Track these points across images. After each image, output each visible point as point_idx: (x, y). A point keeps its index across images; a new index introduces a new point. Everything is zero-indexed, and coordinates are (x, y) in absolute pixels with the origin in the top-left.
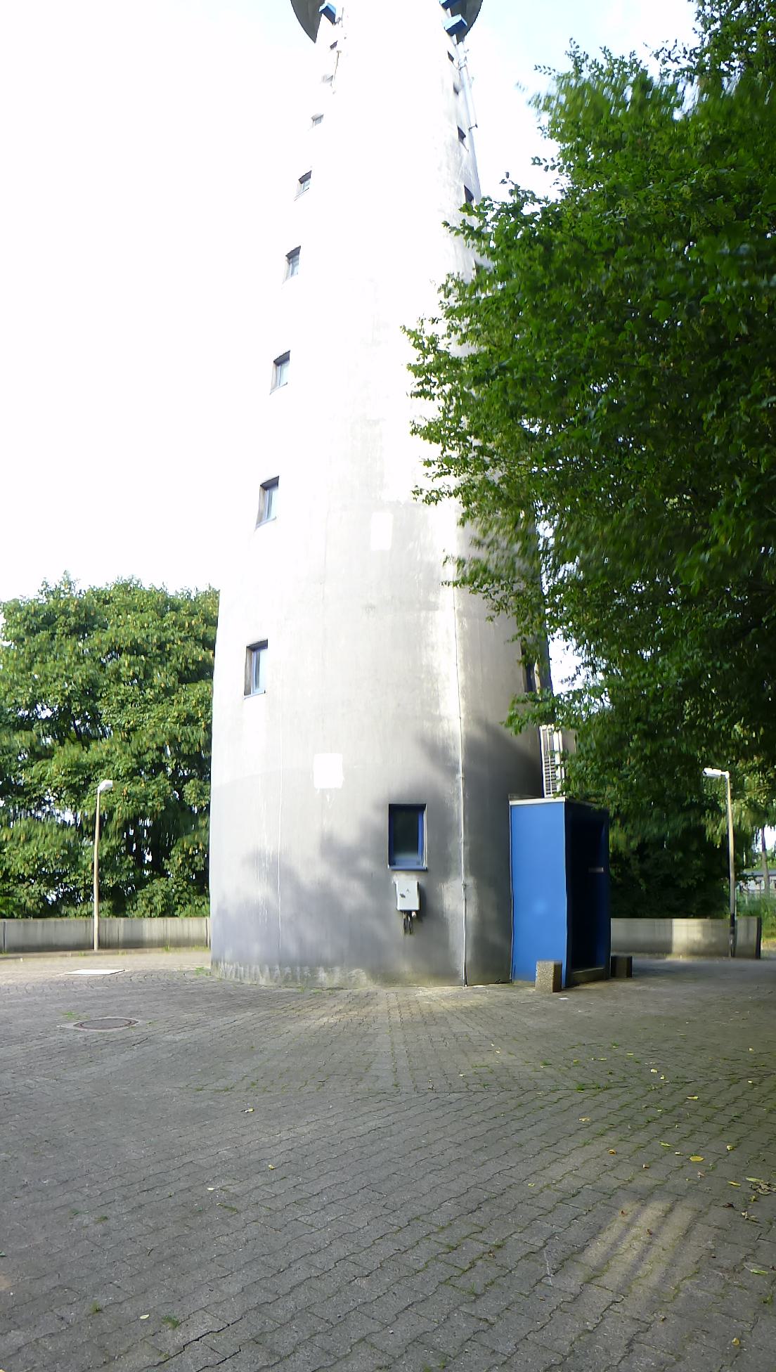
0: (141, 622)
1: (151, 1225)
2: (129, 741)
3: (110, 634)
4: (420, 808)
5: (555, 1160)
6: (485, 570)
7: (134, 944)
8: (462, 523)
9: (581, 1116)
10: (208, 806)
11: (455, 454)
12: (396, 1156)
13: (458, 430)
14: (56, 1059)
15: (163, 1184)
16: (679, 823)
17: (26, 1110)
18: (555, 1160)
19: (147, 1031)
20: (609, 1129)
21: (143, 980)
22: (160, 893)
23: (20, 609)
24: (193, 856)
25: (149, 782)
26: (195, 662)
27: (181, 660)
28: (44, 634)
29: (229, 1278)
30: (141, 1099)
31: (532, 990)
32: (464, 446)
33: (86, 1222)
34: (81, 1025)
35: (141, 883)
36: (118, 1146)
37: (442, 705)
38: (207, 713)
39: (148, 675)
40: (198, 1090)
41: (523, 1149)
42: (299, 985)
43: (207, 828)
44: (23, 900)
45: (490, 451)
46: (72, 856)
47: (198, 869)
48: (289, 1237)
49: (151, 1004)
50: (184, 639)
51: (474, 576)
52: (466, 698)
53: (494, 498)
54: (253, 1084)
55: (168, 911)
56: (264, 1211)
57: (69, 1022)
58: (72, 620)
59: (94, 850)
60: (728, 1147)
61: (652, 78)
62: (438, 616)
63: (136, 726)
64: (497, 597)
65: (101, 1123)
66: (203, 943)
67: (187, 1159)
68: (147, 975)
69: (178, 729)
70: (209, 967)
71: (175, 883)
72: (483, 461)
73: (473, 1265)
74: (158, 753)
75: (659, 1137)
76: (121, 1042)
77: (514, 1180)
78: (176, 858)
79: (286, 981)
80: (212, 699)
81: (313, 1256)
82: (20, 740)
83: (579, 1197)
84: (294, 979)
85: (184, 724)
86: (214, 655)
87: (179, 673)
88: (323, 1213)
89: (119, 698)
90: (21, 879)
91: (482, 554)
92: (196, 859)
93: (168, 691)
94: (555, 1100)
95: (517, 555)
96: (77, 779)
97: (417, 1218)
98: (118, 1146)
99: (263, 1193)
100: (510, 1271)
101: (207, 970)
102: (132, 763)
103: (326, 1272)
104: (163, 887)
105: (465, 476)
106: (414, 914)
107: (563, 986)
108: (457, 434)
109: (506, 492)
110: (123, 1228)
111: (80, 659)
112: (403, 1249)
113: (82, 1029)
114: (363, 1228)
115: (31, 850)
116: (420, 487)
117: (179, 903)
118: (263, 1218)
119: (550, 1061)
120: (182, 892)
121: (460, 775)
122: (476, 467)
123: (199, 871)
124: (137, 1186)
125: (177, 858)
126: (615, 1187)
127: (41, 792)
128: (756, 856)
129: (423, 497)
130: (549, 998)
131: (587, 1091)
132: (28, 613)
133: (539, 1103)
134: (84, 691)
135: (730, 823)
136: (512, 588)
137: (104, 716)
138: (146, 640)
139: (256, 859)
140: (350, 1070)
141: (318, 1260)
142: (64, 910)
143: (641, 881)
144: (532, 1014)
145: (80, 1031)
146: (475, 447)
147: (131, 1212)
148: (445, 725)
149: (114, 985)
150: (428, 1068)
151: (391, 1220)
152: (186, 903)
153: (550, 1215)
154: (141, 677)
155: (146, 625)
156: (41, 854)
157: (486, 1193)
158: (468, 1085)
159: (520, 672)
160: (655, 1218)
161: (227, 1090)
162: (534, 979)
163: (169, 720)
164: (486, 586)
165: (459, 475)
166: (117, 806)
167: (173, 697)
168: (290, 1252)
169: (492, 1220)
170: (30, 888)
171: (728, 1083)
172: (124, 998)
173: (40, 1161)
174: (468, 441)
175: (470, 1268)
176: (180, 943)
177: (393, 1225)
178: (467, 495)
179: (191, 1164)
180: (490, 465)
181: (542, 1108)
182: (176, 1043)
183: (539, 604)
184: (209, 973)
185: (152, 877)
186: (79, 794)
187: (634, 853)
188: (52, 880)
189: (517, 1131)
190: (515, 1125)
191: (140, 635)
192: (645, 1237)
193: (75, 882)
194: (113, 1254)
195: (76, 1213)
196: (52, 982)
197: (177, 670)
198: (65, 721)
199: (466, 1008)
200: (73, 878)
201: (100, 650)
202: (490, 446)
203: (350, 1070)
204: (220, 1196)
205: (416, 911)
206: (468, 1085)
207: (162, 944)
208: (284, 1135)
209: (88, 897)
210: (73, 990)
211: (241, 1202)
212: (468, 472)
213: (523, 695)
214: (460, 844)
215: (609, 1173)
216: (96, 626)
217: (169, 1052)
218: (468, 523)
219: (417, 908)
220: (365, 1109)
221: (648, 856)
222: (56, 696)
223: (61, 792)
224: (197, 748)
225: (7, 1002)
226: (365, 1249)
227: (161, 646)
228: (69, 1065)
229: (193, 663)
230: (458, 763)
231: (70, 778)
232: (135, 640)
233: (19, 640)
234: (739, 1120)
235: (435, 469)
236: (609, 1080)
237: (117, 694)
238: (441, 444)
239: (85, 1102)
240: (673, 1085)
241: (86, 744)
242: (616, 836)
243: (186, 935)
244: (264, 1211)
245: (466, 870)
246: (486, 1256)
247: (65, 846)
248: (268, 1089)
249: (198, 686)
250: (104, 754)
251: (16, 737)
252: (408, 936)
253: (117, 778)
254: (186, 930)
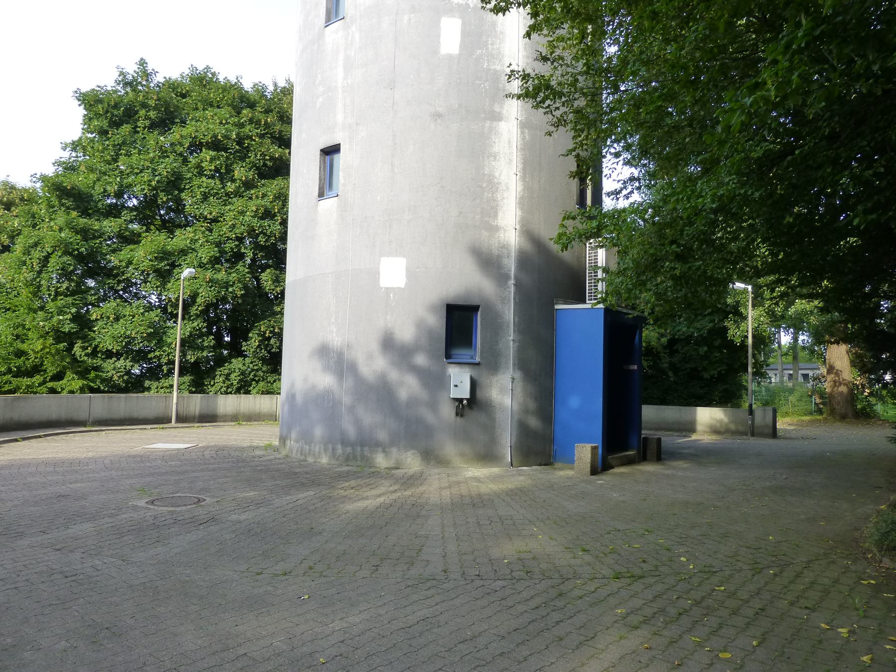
2: (211, 231)
3: (189, 130)
4: (475, 309)
7: (208, 418)
8: (528, 35)
9: (616, 607)
10: (283, 293)
12: (443, 649)
16: (705, 325)
20: (644, 622)
22: (237, 371)
24: (269, 339)
25: (229, 271)
26: (272, 158)
28: (126, 129)
30: (202, 583)
34: (152, 502)
35: (220, 361)
36: (176, 635)
37: (500, 215)
38: (283, 208)
39: (229, 170)
40: (258, 574)
42: (359, 463)
46: (157, 335)
47: (273, 350)
49: (220, 480)
50: (262, 136)
51: (537, 89)
52: (522, 209)
53: (562, 11)
54: (311, 568)
55: (244, 388)
57: (141, 499)
59: (178, 331)
60: (755, 643)
61: (306, 379)
63: (218, 217)
64: (558, 113)
66: (272, 417)
67: (241, 651)
68: (219, 449)
69: (256, 223)
70: (276, 442)
74: (237, 243)
75: (690, 630)
76: (188, 521)
78: (253, 340)
79: (347, 459)
82: (110, 225)
84: (355, 458)
85: (262, 218)
86: (290, 153)
87: (258, 168)
89: (202, 190)
90: (109, 354)
91: (545, 69)
92: (272, 341)
95: (580, 73)
96: (163, 264)
98: (176, 635)
101: (275, 446)
102: (215, 251)
104: (240, 366)
106: (465, 402)
107: (599, 469)
113: (152, 507)
115: (119, 328)
117: (253, 380)
119: (588, 547)
121: (512, 282)
123: (274, 352)
125: (253, 342)
127: (129, 275)
128: (773, 351)
131: (623, 580)
133: (577, 593)
135: (750, 325)
136: (572, 106)
137: (188, 206)
138: (227, 137)
139: (323, 351)
142: (147, 383)
143: (671, 374)
145: (150, 509)
150: (476, 553)
152: (259, 380)
158: (512, 571)
163: (248, 213)
164: (548, 102)
166: (200, 291)
167: (252, 192)
171: (753, 572)
172: (196, 474)
173: (98, 651)
176: (251, 418)
182: (241, 522)
184: (276, 450)
185: (231, 356)
187: (665, 348)
189: (557, 623)
190: (556, 616)
191: (220, 131)
196: (129, 456)
197: (255, 166)
198: (150, 210)
199: (511, 490)
200: (157, 353)
201: (181, 144)
205: (467, 399)
206: (512, 571)
207: (235, 418)
208: (337, 625)
209: (170, 372)
210: (149, 464)
213: (574, 208)
214: (510, 341)
216: (178, 120)
217: (233, 532)
219: (468, 397)
220: (415, 597)
221: (677, 351)
222: (143, 187)
223: (148, 274)
224: (272, 240)
227: (240, 142)
229: (270, 160)
230: (511, 271)
231: (156, 263)
232: (215, 136)
233: (103, 133)
234: (763, 613)
236: (642, 569)
239: (148, 585)
240: (701, 575)
242: (650, 334)
243: (258, 410)
245: (514, 365)
247: (151, 325)
248: (324, 574)
249: (276, 182)
250: (188, 241)
252: (458, 419)
253: (201, 265)
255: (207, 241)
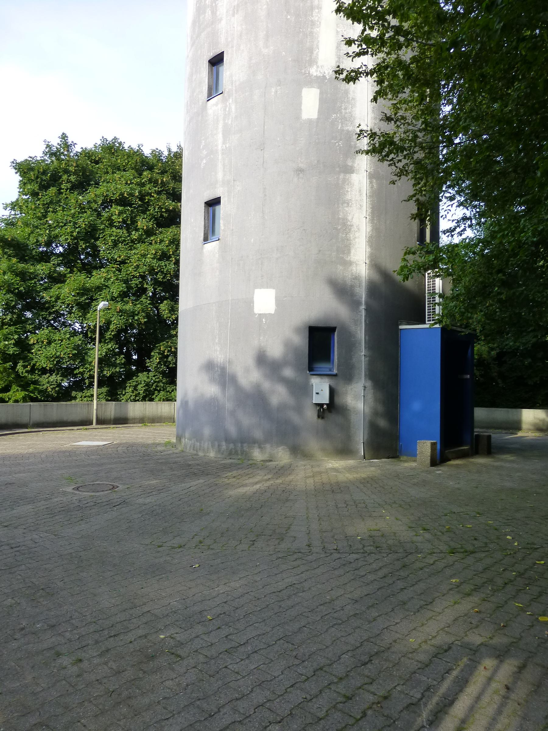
0: (125, 179)
1: (114, 668)
2: (120, 271)
3: (102, 189)
5: (431, 618)
6: (392, 143)
8: (375, 99)
9: (451, 577)
10: (177, 319)
11: (374, 34)
12: (307, 610)
13: (380, 9)
14: (57, 517)
15: (126, 631)
17: (30, 561)
18: (431, 618)
19: (125, 494)
20: (475, 590)
21: (126, 451)
22: (143, 383)
23: (32, 169)
24: (167, 356)
26: (167, 211)
27: (156, 210)
28: (52, 190)
29: (171, 720)
30: (115, 554)
31: (414, 464)
32: (383, 26)
33: (65, 663)
34: (77, 489)
35: (130, 375)
36: (95, 595)
38: (176, 251)
39: (134, 222)
40: (159, 547)
41: (406, 607)
42: (240, 457)
43: (176, 336)
44: (45, 387)
45: (406, 30)
48: (220, 682)
49: (130, 471)
50: (159, 193)
51: (383, 145)
52: (371, 246)
53: (404, 78)
54: (201, 542)
55: (148, 396)
56: (201, 658)
58: (73, 178)
62: (354, 177)
63: (125, 260)
64: (400, 165)
65: (84, 574)
67: (146, 609)
70: (174, 440)
71: (154, 376)
72: (398, 40)
73: (364, 714)
76: (105, 504)
77: (398, 635)
78: (155, 358)
79: (230, 453)
80: (180, 239)
81: (238, 702)
83: (451, 652)
85: (160, 259)
87: (156, 219)
88: (247, 661)
89: (113, 238)
90: (44, 371)
91: (390, 128)
93: (149, 233)
94: (432, 562)
96: (83, 299)
97: (321, 669)
99: (201, 642)
100: (394, 722)
102: (123, 287)
103: (247, 717)
104: (145, 379)
105: (381, 55)
106: (325, 406)
108: (378, 12)
109: (415, 71)
110: (92, 670)
111: (82, 209)
112: (309, 697)
113: (77, 492)
114: (278, 677)
115: (51, 350)
116: (341, 67)
118: (200, 665)
119: (427, 527)
120: (158, 382)
121: (363, 307)
122: (390, 46)
123: (172, 367)
124: (106, 632)
125: (156, 358)
126: (479, 643)
127: (57, 308)
129: (343, 76)
130: (427, 471)
131: (457, 555)
132: (39, 172)
133: (418, 565)
134: (86, 233)
136: (413, 158)
140: (274, 531)
141: (242, 705)
142: (74, 393)
144: (414, 484)
146: (393, 27)
147: (101, 655)
148: (354, 268)
149: (104, 454)
151: (301, 670)
153: (426, 669)
154: (129, 222)
155: (129, 182)
156: (59, 353)
157: (376, 647)
158: (364, 546)
159: (415, 224)
160: (511, 674)
161: (181, 547)
162: (415, 455)
163: (149, 256)
164: (392, 156)
165: (376, 55)
166: (113, 319)
167: (152, 238)
168: (220, 697)
169: (380, 672)
170: (50, 378)
172: (109, 466)
173: (36, 607)
174: (386, 20)
175: (362, 718)
177: (302, 675)
178: (381, 74)
179: (149, 614)
180: (404, 44)
181: (421, 569)
183: (433, 170)
184: (174, 446)
185: (138, 371)
186: (84, 309)
188: (68, 372)
189: (402, 589)
190: (400, 584)
191: (126, 190)
192: (503, 692)
193: (82, 374)
194: (83, 694)
195: (58, 654)
200: (81, 370)
201: (95, 202)
202: (406, 25)
203: (274, 531)
204: (169, 643)
206: (364, 546)
207: (142, 421)
208: (222, 589)
209: (91, 385)
210: (75, 458)
211: (185, 649)
212: (383, 51)
215: (474, 630)
218: (380, 100)
222: (67, 237)
223: (72, 307)
225: (26, 468)
226: (279, 696)
227: (142, 197)
228: (66, 523)
231: (78, 298)
232: (122, 194)
233: (34, 194)
235: (355, 48)
237: (111, 236)
238: (362, 25)
241: (89, 273)
244: (201, 658)
245: (365, 375)
246: (375, 706)
247: (77, 347)
249: (170, 230)
251: (38, 267)
252: (320, 421)
253: (113, 299)
254: (159, 410)
255: (117, 279)
